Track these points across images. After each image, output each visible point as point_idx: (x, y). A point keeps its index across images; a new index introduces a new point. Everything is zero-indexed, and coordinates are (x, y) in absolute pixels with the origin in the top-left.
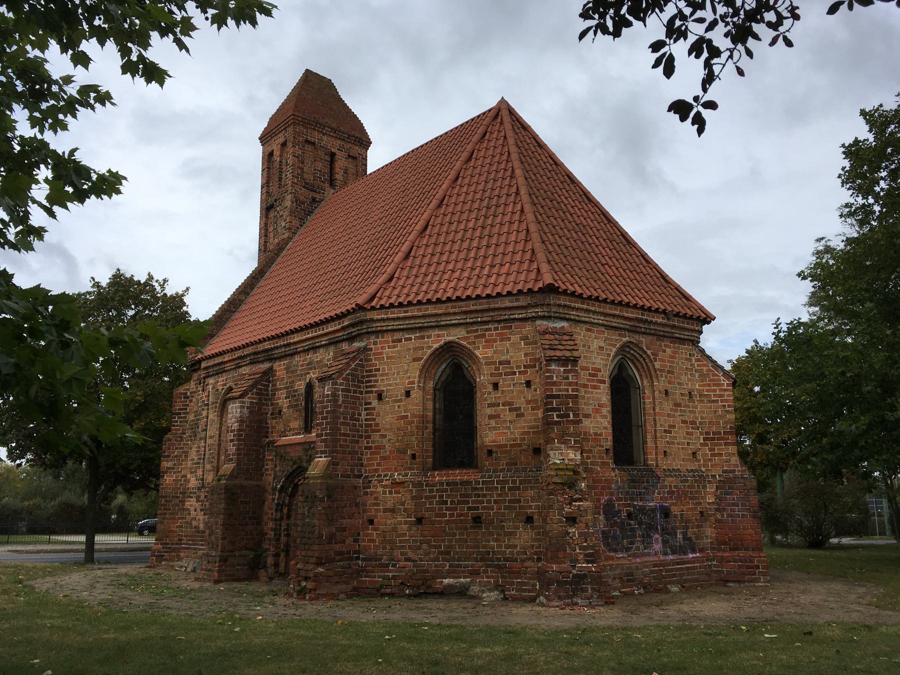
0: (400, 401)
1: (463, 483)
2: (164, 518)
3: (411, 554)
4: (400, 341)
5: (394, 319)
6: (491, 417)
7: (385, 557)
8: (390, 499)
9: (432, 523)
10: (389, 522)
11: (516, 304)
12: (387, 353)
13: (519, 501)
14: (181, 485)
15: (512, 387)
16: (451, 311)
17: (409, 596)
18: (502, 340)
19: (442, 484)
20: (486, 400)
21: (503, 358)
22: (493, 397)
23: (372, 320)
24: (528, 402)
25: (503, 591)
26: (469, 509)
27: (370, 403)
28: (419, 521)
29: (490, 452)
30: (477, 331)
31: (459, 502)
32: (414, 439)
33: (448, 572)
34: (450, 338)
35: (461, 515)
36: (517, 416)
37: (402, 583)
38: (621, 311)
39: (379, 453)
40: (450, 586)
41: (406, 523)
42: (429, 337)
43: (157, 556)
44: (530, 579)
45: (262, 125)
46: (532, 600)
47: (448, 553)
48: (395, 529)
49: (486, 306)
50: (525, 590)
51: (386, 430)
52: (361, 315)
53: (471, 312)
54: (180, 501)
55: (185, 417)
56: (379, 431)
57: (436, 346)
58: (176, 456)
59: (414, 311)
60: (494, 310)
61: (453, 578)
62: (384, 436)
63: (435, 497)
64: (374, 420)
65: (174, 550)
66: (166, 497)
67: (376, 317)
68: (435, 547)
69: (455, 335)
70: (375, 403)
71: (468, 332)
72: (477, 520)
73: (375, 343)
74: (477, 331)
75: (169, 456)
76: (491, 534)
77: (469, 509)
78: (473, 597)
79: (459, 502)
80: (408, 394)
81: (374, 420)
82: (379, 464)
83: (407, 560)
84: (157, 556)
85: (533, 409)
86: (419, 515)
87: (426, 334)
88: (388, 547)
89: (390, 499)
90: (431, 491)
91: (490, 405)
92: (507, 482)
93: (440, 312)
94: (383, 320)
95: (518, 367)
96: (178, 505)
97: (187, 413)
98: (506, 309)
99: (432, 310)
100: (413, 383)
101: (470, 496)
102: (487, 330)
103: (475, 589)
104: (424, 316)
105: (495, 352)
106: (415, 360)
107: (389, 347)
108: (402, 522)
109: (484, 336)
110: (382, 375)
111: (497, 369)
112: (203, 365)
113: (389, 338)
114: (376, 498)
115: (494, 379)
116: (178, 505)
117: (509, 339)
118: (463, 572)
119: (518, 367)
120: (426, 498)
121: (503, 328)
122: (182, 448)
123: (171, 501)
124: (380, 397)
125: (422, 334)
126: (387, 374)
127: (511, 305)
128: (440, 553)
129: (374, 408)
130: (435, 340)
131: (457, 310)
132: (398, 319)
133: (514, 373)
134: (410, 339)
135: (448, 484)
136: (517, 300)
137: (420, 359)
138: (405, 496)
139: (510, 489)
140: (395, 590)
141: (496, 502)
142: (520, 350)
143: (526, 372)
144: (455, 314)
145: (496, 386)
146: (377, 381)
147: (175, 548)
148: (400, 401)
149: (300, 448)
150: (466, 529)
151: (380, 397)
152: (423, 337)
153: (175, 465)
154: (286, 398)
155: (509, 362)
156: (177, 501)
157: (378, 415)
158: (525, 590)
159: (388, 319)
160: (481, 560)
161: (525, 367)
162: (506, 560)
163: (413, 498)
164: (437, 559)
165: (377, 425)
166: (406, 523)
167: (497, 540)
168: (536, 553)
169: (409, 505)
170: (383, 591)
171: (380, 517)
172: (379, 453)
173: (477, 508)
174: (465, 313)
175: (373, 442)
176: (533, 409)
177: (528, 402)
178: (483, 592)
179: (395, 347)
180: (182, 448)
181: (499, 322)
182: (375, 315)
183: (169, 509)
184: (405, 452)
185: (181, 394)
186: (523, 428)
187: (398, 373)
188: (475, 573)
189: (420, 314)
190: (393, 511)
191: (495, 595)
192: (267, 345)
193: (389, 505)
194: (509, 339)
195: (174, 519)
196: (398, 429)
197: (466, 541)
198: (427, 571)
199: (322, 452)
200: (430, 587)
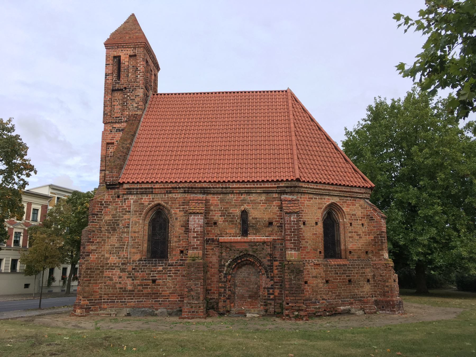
0: (313, 226)
1: (344, 265)
2: (89, 283)
3: (325, 297)
4: (312, 198)
5: (311, 188)
6: (350, 237)
7: (313, 299)
8: (314, 272)
9: (333, 283)
10: (314, 282)
11: (360, 191)
12: (307, 203)
13: (364, 273)
14: (101, 261)
15: (357, 224)
16: (336, 189)
17: (328, 315)
18: (353, 205)
19: (335, 265)
20: (348, 230)
21: (353, 213)
22: (350, 229)
23: (302, 187)
24: (363, 232)
25: (364, 311)
26: (347, 276)
27: (300, 226)
28: (327, 282)
29: (350, 252)
30: (343, 200)
31: (343, 274)
32: (320, 244)
33: (341, 304)
34: (333, 201)
35: (344, 279)
36: (360, 237)
37: (324, 310)
38: (261, 185)
39: (305, 250)
40: (344, 310)
41: (322, 282)
42: (324, 199)
43: (86, 309)
44: (371, 304)
45: (107, 36)
46: (375, 313)
47: (340, 296)
48: (317, 286)
49: (349, 190)
50: (372, 309)
51: (308, 239)
52: (297, 184)
53: (342, 191)
54: (101, 272)
55: (101, 217)
56: (304, 239)
57: (328, 203)
58: (98, 242)
59: (320, 186)
60: (351, 192)
61: (344, 306)
62: (307, 242)
63: (333, 271)
64: (302, 234)
65: (98, 303)
66: (91, 269)
67: (304, 186)
68: (334, 293)
69: (335, 200)
70: (302, 226)
71: (340, 200)
72: (350, 281)
73: (301, 198)
74: (343, 200)
75: (93, 242)
76: (355, 287)
77: (347, 276)
78: (353, 314)
79: (343, 274)
80: (316, 223)
81: (302, 234)
82: (305, 255)
83: (323, 299)
84: (86, 309)
85: (365, 235)
86: (327, 279)
87: (323, 197)
88: (315, 294)
89: (314, 272)
90: (331, 268)
91: (350, 232)
92: (359, 265)
93: (331, 189)
94: (306, 188)
95: (359, 217)
96: (99, 274)
97: (102, 215)
98: (357, 193)
99: (328, 187)
100: (319, 219)
101: (346, 271)
102: (347, 200)
103: (353, 311)
104: (324, 190)
105: (350, 210)
106: (319, 208)
107: (307, 201)
108: (320, 282)
109: (346, 202)
110: (305, 213)
111: (351, 217)
112: (125, 186)
113: (307, 196)
114: (308, 271)
115: (350, 221)
116: (99, 274)
117: (355, 205)
118: (347, 303)
119: (359, 217)
120: (330, 271)
121: (353, 200)
122: (101, 237)
123: (94, 272)
124: (304, 224)
125: (321, 197)
126: (307, 213)
127: (359, 191)
128: (336, 296)
129: (302, 229)
130: (328, 201)
131: (337, 189)
132: (313, 188)
133: (358, 220)
134: (316, 198)
135: (338, 265)
136: (360, 190)
137: (321, 208)
138: (321, 270)
139: (361, 268)
140: (322, 313)
141: (356, 273)
142: (359, 210)
143: (362, 220)
144: (336, 191)
145: (351, 224)
146: (303, 216)
147: (97, 303)
148: (313, 226)
149: (247, 245)
150: (346, 285)
151: (304, 224)
152: (322, 199)
153: (97, 248)
154: (221, 216)
155: (355, 215)
156: (98, 272)
157: (304, 232)
158: (372, 309)
159: (309, 188)
160: (352, 298)
161: (361, 218)
162: (361, 297)
163: (324, 271)
164: (335, 299)
165: (304, 237)
166: (322, 282)
167: (358, 289)
168: (371, 294)
169: (323, 274)
170: (317, 314)
171: (310, 281)
172: (305, 250)
173: (349, 276)
174: (340, 191)
175: (302, 245)
176: (365, 235)
177: (363, 232)
178: (356, 311)
179: (310, 201)
180: (101, 237)
181: (352, 197)
182: (301, 184)
183: (93, 277)
184: (317, 250)
185: (99, 202)
186: (362, 243)
187: (312, 213)
188: (351, 304)
189: (323, 188)
190: (316, 277)
191: (361, 312)
192: (204, 185)
193: (314, 274)
194: (355, 205)
195: (96, 283)
196: (313, 239)
197: (346, 290)
198: (333, 304)
199: (291, 249)
200: (336, 311)
